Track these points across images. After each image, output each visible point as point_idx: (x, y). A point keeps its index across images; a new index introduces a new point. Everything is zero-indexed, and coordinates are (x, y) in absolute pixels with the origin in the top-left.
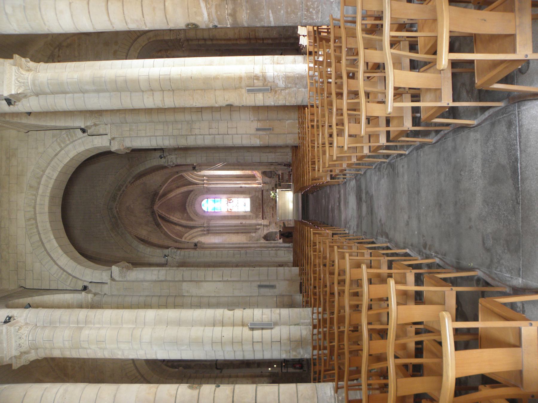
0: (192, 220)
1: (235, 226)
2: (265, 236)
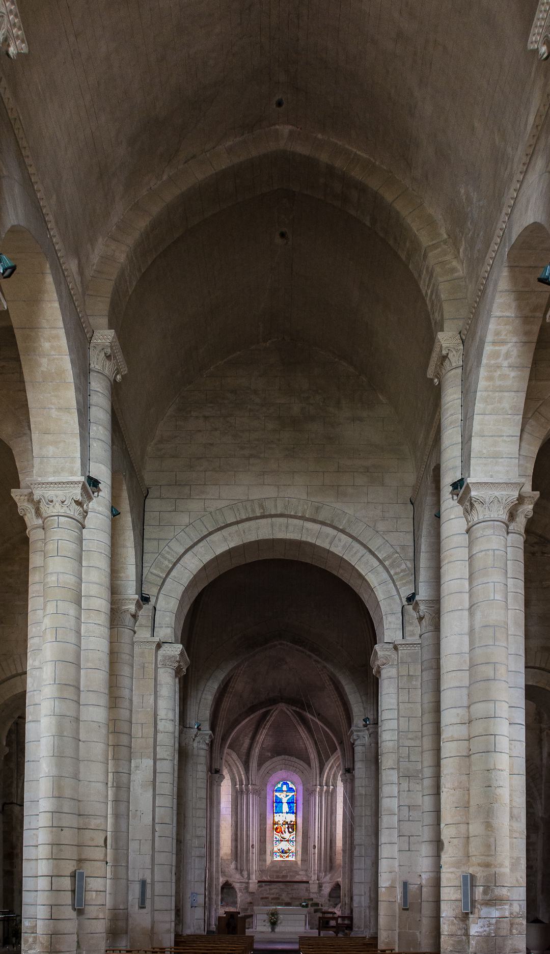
0: (260, 765)
2: (230, 885)
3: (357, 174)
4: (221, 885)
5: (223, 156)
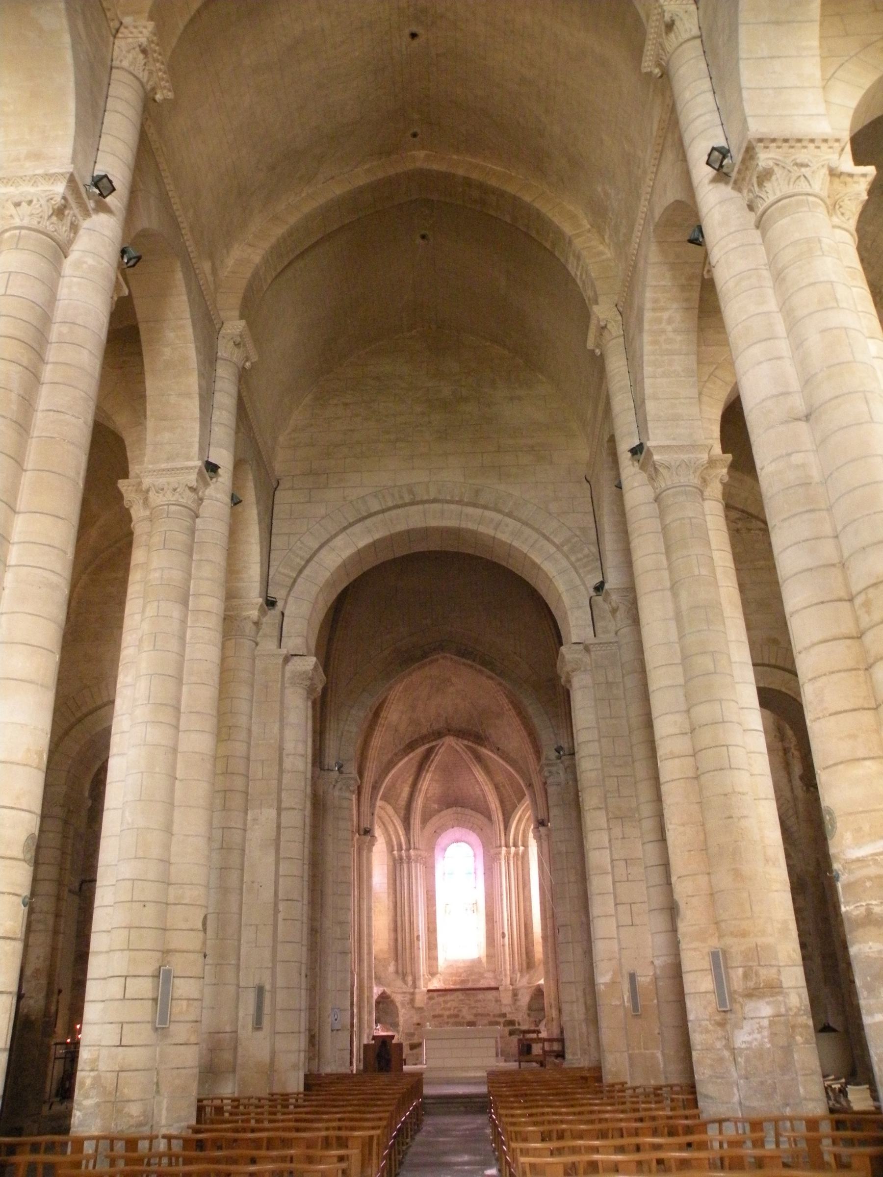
0: (424, 821)
1: (411, 923)
3: (493, 182)
4: (375, 997)
5: (361, 176)
